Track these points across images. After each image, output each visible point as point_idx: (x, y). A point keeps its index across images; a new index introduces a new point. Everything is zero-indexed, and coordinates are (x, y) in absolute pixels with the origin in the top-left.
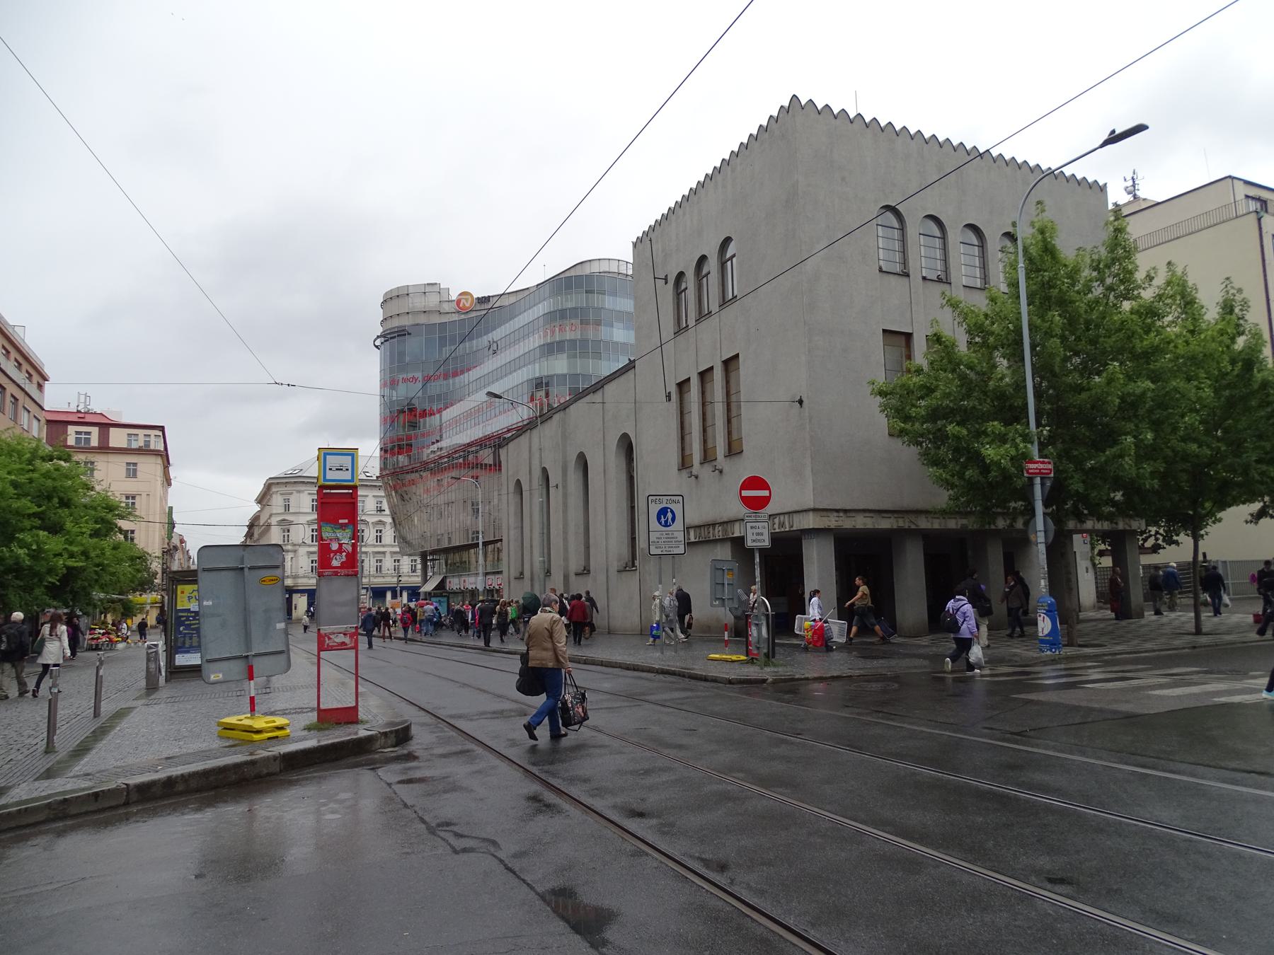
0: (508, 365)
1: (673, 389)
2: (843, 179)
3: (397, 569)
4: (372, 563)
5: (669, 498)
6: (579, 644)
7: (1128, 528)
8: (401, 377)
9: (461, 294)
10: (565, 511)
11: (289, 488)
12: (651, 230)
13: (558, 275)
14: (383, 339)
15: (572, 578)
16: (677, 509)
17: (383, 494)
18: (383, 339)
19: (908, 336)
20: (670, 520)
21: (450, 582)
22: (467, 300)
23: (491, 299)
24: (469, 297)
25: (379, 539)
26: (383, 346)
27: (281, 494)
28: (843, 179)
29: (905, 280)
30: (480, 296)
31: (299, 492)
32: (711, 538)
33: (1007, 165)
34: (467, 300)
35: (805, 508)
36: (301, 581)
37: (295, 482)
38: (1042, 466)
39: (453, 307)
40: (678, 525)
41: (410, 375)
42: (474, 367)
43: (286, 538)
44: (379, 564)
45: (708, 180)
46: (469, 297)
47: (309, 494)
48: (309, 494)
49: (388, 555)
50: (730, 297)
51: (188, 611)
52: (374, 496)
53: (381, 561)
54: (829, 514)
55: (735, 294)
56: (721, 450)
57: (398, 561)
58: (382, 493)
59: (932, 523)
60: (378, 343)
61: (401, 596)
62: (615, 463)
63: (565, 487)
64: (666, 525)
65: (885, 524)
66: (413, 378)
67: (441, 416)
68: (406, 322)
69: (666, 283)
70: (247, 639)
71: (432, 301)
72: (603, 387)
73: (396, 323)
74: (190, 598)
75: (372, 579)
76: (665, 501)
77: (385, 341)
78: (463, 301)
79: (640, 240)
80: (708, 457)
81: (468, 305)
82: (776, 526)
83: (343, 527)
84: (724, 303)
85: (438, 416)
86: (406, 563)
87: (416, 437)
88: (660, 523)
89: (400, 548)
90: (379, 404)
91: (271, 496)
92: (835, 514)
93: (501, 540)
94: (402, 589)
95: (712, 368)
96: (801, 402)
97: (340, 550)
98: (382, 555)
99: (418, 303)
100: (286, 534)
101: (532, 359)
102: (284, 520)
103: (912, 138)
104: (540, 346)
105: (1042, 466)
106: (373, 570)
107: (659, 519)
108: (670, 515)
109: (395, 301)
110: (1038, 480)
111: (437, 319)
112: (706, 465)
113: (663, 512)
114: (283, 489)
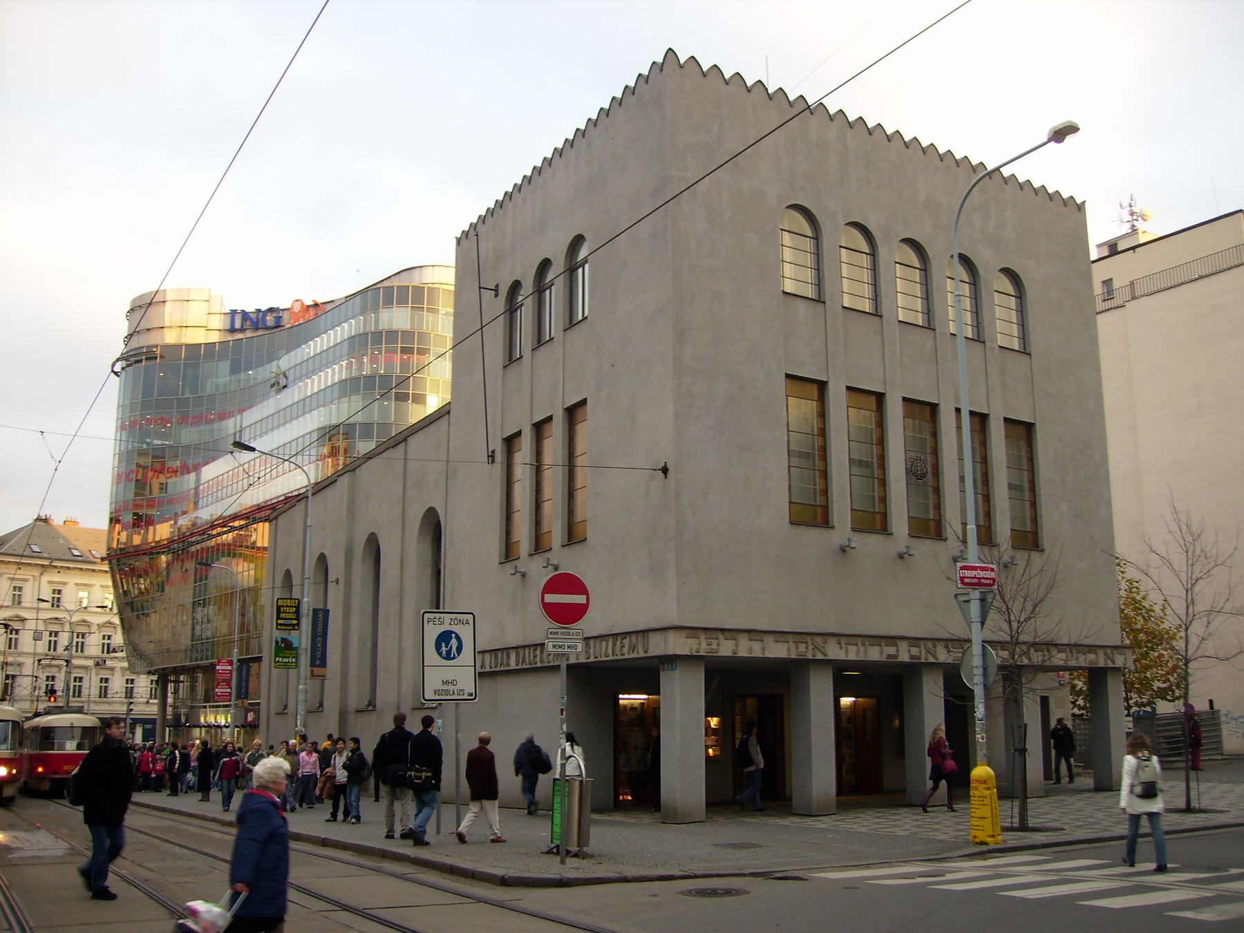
0: (313, 407)
1: (498, 446)
3: (130, 693)
4: (93, 683)
5: (453, 616)
7: (1111, 665)
12: (481, 222)
13: (374, 285)
14: (124, 363)
15: (352, 718)
16: (465, 632)
18: (124, 363)
19: (880, 397)
20: (454, 649)
26: (123, 373)
29: (821, 306)
32: (539, 665)
35: (666, 624)
40: (467, 655)
42: (250, 408)
44: (104, 685)
45: (557, 155)
50: (580, 318)
53: (107, 680)
55: (586, 314)
57: (132, 681)
59: (847, 652)
60: (118, 368)
62: (417, 547)
64: (448, 657)
65: (778, 651)
69: (496, 296)
76: (447, 621)
77: (128, 366)
79: (466, 234)
82: (625, 650)
84: (571, 323)
85: (193, 476)
86: (144, 684)
88: (440, 654)
89: (129, 662)
93: (259, 659)
94: (135, 722)
95: (550, 419)
96: (665, 470)
98: (109, 672)
101: (328, 400)
103: (831, 118)
105: (982, 574)
106: (95, 691)
107: (438, 647)
108: (454, 642)
112: (535, 558)
113: (445, 637)
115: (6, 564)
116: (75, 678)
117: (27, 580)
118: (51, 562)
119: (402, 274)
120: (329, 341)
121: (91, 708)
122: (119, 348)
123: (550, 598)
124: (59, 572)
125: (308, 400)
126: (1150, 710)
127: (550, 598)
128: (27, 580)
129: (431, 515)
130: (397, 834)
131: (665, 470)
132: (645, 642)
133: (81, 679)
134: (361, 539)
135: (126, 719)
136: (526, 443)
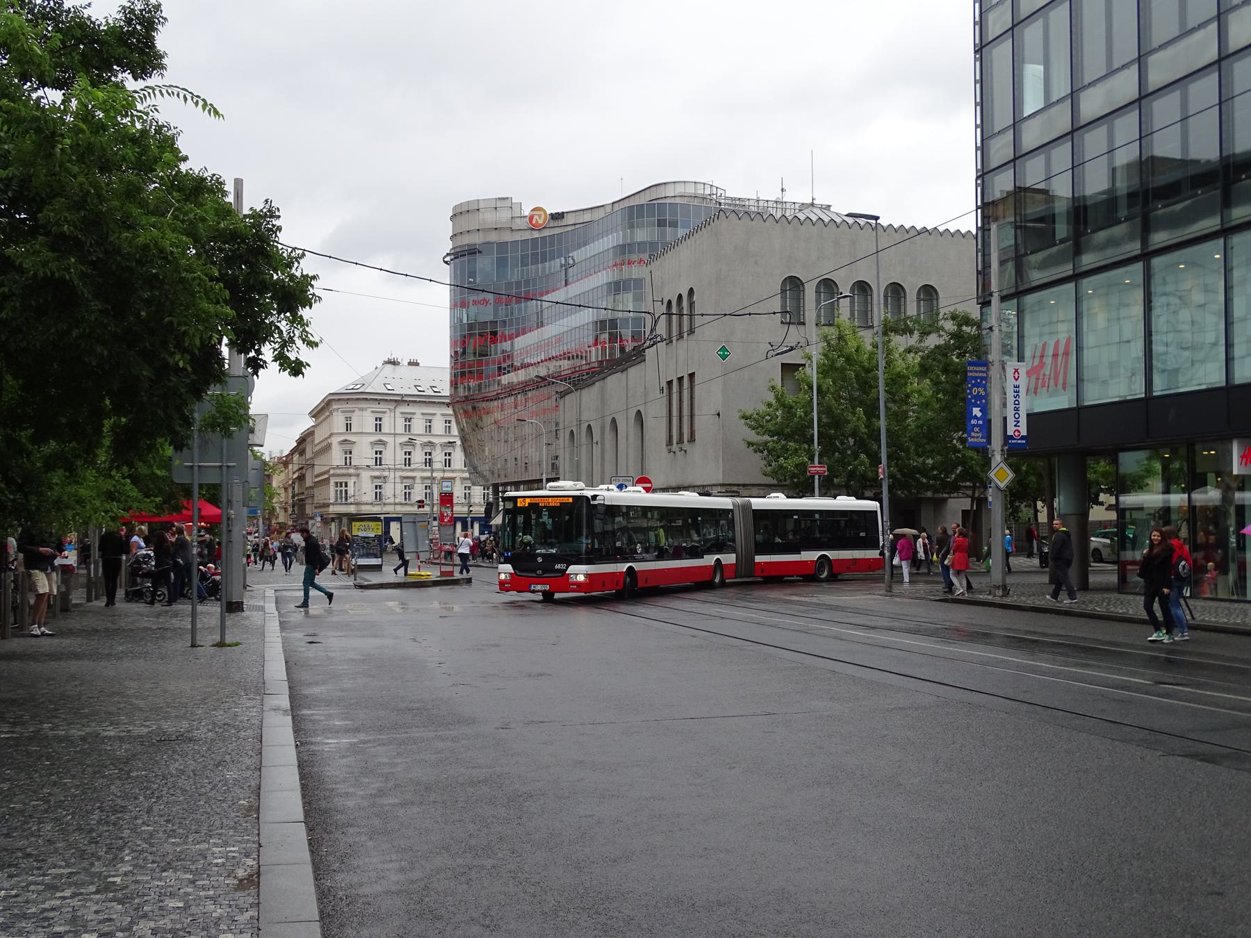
1: (664, 385)
2: (756, 263)
9: (533, 210)
10: (603, 465)
11: (350, 406)
17: (451, 412)
18: (452, 257)
22: (540, 216)
23: (565, 215)
24: (542, 213)
25: (448, 463)
27: (342, 412)
28: (756, 263)
30: (554, 212)
31: (362, 409)
33: (896, 232)
34: (540, 216)
37: (357, 399)
43: (348, 463)
47: (373, 412)
48: (373, 412)
49: (458, 482)
52: (442, 415)
56: (686, 437)
58: (450, 411)
60: (448, 259)
61: (472, 527)
63: (603, 444)
67: (512, 343)
68: (476, 239)
71: (504, 216)
72: (627, 369)
73: (466, 240)
77: (455, 258)
78: (535, 217)
80: (680, 441)
81: (541, 222)
83: (448, 507)
87: (487, 364)
89: (470, 473)
91: (331, 413)
94: (474, 519)
96: (719, 415)
97: (447, 516)
99: (489, 218)
100: (348, 456)
102: (346, 440)
104: (607, 284)
105: (819, 469)
109: (465, 217)
110: (817, 477)
111: (508, 237)
117: (385, 412)
120: (608, 242)
122: (448, 246)
125: (573, 331)
126: (572, 569)
128: (385, 412)
129: (639, 413)
130: (279, 594)
132: (719, 489)
134: (609, 420)
136: (675, 384)
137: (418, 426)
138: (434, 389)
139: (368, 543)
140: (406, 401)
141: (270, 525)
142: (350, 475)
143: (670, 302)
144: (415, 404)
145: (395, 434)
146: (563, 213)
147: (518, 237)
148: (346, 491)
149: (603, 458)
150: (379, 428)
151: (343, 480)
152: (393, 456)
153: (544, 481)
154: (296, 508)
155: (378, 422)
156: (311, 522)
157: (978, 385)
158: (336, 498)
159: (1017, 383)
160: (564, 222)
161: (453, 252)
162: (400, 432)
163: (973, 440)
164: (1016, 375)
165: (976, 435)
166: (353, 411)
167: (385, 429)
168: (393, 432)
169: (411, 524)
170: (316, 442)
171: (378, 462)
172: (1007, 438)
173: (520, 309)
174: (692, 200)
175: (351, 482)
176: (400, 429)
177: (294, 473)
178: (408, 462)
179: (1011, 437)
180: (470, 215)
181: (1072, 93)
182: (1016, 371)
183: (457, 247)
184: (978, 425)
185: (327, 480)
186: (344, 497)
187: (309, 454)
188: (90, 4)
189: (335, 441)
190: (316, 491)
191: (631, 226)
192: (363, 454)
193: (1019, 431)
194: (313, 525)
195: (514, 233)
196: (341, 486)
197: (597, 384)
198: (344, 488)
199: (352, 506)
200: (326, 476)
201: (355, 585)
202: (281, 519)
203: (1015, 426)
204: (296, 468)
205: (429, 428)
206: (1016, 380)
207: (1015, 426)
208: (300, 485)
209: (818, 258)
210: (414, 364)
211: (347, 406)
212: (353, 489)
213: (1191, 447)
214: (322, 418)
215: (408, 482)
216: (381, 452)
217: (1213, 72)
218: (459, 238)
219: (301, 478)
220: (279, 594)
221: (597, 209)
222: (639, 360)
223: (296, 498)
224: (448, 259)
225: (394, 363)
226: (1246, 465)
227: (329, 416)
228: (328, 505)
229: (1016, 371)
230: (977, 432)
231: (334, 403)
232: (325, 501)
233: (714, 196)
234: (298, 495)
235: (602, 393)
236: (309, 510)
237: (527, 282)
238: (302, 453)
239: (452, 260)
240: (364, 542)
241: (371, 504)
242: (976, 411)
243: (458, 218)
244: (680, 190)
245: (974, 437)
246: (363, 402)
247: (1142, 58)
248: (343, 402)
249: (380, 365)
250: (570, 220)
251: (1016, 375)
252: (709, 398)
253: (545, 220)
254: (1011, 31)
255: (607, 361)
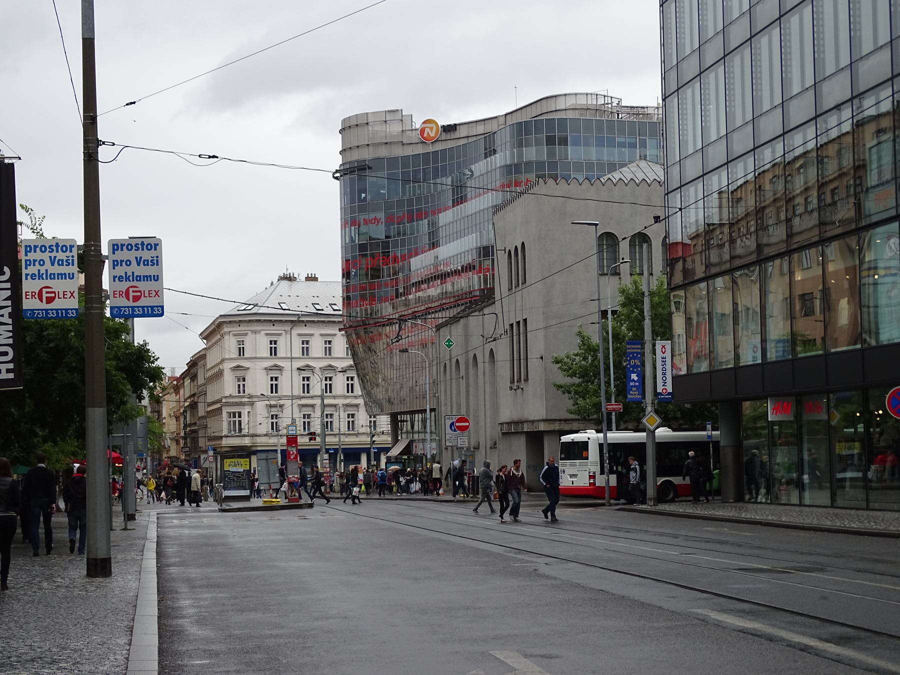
1: (507, 327)
6: (515, 512)
8: (362, 218)
11: (243, 328)
21: (416, 446)
22: (431, 129)
23: (458, 127)
24: (434, 125)
26: (342, 178)
27: (235, 335)
30: (446, 124)
31: (255, 332)
34: (431, 129)
36: (259, 440)
37: (250, 321)
38: (615, 407)
39: (415, 137)
41: (372, 216)
43: (241, 389)
46: (434, 125)
47: (267, 334)
48: (267, 334)
51: (229, 471)
53: (353, 416)
54: (554, 422)
63: (467, 379)
66: (375, 219)
68: (366, 155)
70: (269, 479)
71: (395, 128)
73: (356, 156)
74: (229, 465)
75: (343, 438)
80: (519, 380)
81: (432, 135)
83: (294, 447)
86: (384, 422)
87: (379, 286)
88: (452, 430)
90: (340, 247)
91: (222, 336)
92: (558, 422)
99: (379, 131)
102: (239, 366)
105: (615, 407)
106: (344, 428)
109: (354, 131)
110: (614, 413)
111: (399, 152)
114: (236, 329)
115: (262, 322)
116: (327, 415)
117: (280, 335)
118: (299, 318)
119: (543, 101)
121: (342, 440)
122: (336, 162)
123: (467, 424)
124: (306, 325)
127: (467, 424)
128: (280, 335)
131: (542, 358)
133: (331, 415)
134: (471, 356)
135: (370, 448)
137: (317, 347)
138: (334, 306)
139: (237, 477)
140: (303, 321)
141: (160, 460)
142: (242, 404)
143: (510, 251)
144: (313, 325)
145: (292, 358)
146: (455, 125)
147: (409, 151)
148: (240, 422)
149: (468, 392)
150: (274, 352)
151: (236, 409)
152: (289, 384)
153: (428, 411)
154: (188, 440)
155: (273, 346)
156: (202, 457)
157: (634, 358)
158: (230, 431)
159: (664, 356)
160: (457, 135)
161: (342, 168)
162: (298, 356)
163: (632, 397)
164: (663, 350)
165: (634, 393)
166: (246, 334)
167: (281, 353)
168: (290, 356)
169: (264, 461)
170: (208, 366)
171: (274, 388)
172: (656, 394)
173: (412, 227)
174: (584, 112)
175: (245, 411)
176: (297, 353)
177: (185, 401)
178: (307, 388)
179: (660, 394)
180: (360, 129)
181: (891, 40)
182: (663, 347)
183: (346, 163)
184: (635, 386)
185: (220, 409)
186: (236, 428)
187: (201, 380)
188: (44, 217)
189: (227, 366)
190: (210, 422)
191: (520, 145)
192: (258, 383)
193: (666, 389)
194: (205, 459)
195: (405, 147)
196: (235, 417)
197: (462, 320)
198: (237, 419)
199: (246, 438)
200: (218, 406)
201: (219, 509)
202: (173, 453)
203: (663, 386)
204: (187, 395)
205: (328, 351)
206: (664, 353)
207: (663, 386)
208: (193, 415)
209: (631, 215)
210: (312, 279)
211: (239, 329)
212: (247, 419)
213: (735, 406)
214: (214, 341)
215: (307, 411)
216: (276, 379)
217: (888, 88)
218: (348, 153)
219: (193, 406)
220: (158, 516)
221: (490, 121)
222: (490, 302)
223: (188, 429)
224: (338, 175)
225: (289, 278)
226: (776, 414)
227: (220, 339)
228: (221, 438)
229: (663, 347)
230: (635, 391)
231: (225, 326)
232: (217, 435)
233: (610, 106)
234: (190, 425)
235: (466, 327)
236: (202, 443)
237: (419, 199)
238: (194, 378)
239: (341, 176)
240: (234, 476)
241: (266, 435)
242: (634, 377)
243: (347, 132)
244: (570, 102)
245: (632, 395)
246: (255, 324)
247: (893, 42)
248: (235, 325)
249: (275, 281)
250: (462, 132)
251: (663, 350)
252: (537, 345)
253: (436, 133)
254: (779, 21)
255: (487, 289)
